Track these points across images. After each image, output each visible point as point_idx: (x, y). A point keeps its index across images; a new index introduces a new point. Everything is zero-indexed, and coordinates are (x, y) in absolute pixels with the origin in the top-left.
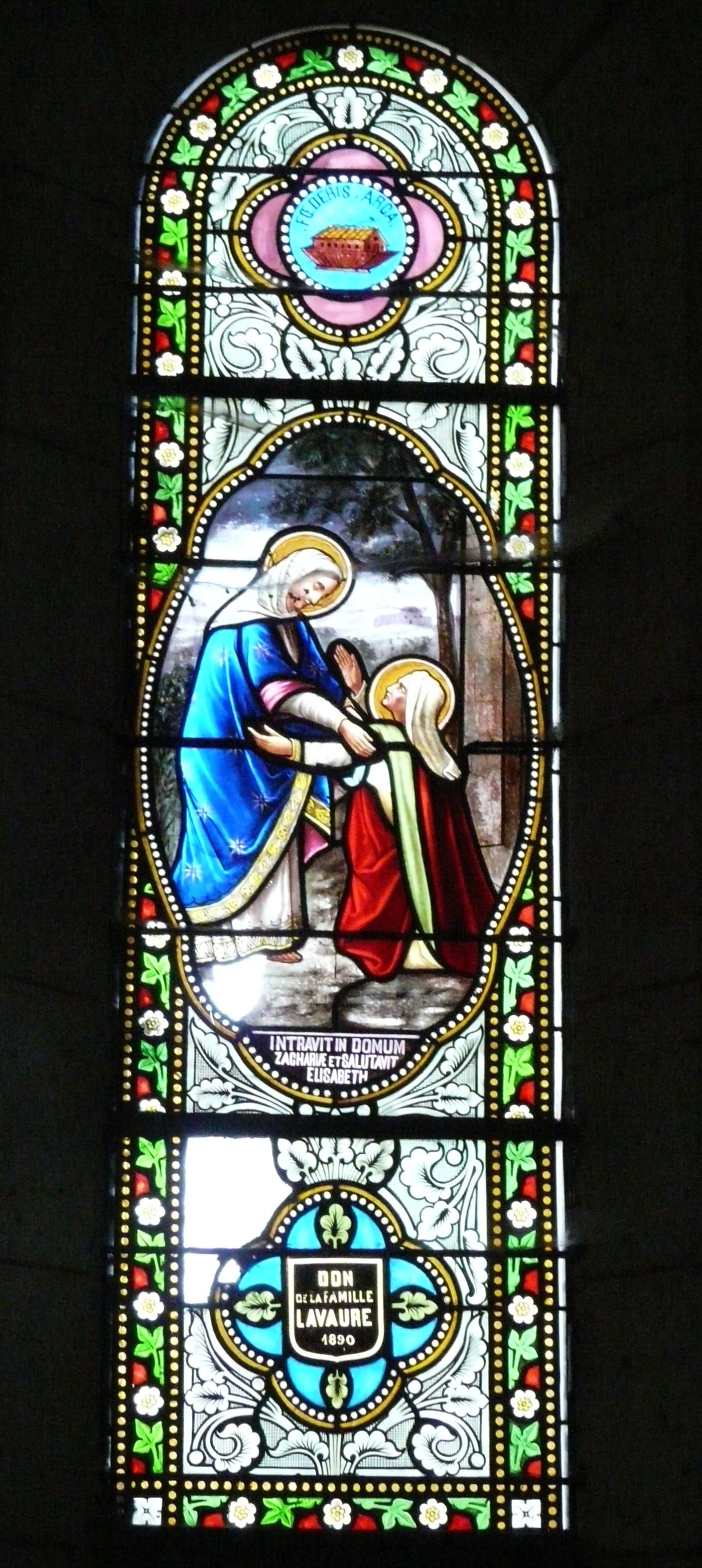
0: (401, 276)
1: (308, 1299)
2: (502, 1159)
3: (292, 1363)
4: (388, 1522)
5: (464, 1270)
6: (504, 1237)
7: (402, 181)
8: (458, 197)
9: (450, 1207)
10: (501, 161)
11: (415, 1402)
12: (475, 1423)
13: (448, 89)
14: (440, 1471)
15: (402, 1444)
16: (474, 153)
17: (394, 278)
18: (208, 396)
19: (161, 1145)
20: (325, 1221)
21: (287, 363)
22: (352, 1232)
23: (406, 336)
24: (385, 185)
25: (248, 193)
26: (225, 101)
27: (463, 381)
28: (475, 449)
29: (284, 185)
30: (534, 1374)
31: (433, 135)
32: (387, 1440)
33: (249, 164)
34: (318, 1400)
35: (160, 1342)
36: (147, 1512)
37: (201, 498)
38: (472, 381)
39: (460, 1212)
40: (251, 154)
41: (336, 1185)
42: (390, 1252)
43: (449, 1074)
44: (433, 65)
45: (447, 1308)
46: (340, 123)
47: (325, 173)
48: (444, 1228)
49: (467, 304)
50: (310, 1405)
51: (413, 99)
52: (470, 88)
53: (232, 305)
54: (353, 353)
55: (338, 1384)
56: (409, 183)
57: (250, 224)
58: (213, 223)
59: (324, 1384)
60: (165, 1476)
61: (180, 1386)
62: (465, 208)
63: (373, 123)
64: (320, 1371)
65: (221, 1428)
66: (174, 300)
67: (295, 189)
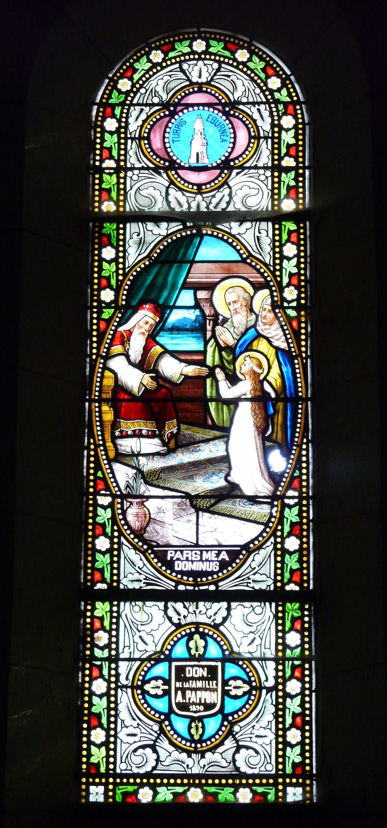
0: (227, 158)
1: (183, 685)
2: (284, 612)
3: (173, 717)
4: (221, 798)
5: (262, 667)
6: (284, 651)
7: (229, 108)
8: (256, 116)
9: (257, 636)
10: (277, 95)
11: (236, 736)
12: (268, 748)
13: (250, 60)
14: (249, 771)
15: (230, 759)
16: (263, 92)
17: (223, 158)
18: (128, 222)
19: (107, 604)
20: (192, 644)
21: (168, 203)
22: (205, 647)
23: (230, 187)
24: (219, 111)
25: (148, 117)
26: (135, 70)
27: (259, 210)
28: (266, 242)
29: (167, 113)
30: (301, 721)
31: (243, 85)
32: (222, 758)
33: (149, 102)
34: (187, 736)
35: (114, 269)
36: (97, 794)
37: (125, 275)
38: (264, 210)
39: (261, 639)
40: (150, 97)
41: (197, 625)
42: (224, 660)
43: (255, 568)
44: (242, 48)
45: (256, 688)
46: (195, 79)
47: (188, 106)
48: (253, 648)
49: (261, 171)
50: (183, 738)
51: (232, 65)
52: (261, 59)
53: (140, 175)
54: (203, 198)
55: (197, 727)
56: (230, 110)
57: (149, 133)
58: (130, 134)
59: (190, 727)
60: (107, 775)
61: (115, 729)
62: (259, 123)
63: (212, 79)
64: (188, 721)
65: (135, 751)
66: (110, 174)
67: (172, 114)
